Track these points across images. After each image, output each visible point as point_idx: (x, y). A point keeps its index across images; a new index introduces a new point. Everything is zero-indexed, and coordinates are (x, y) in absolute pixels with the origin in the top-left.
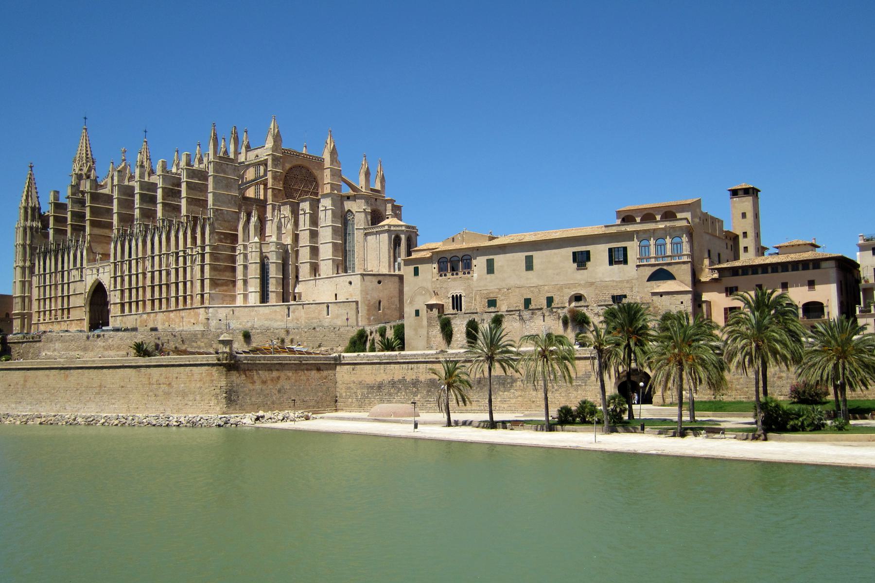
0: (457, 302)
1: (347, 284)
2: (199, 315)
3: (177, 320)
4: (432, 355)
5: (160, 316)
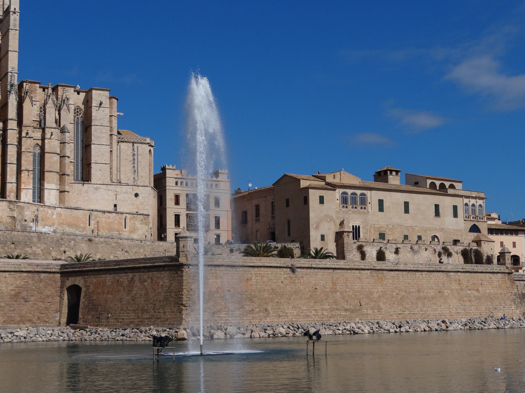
1: (140, 197)
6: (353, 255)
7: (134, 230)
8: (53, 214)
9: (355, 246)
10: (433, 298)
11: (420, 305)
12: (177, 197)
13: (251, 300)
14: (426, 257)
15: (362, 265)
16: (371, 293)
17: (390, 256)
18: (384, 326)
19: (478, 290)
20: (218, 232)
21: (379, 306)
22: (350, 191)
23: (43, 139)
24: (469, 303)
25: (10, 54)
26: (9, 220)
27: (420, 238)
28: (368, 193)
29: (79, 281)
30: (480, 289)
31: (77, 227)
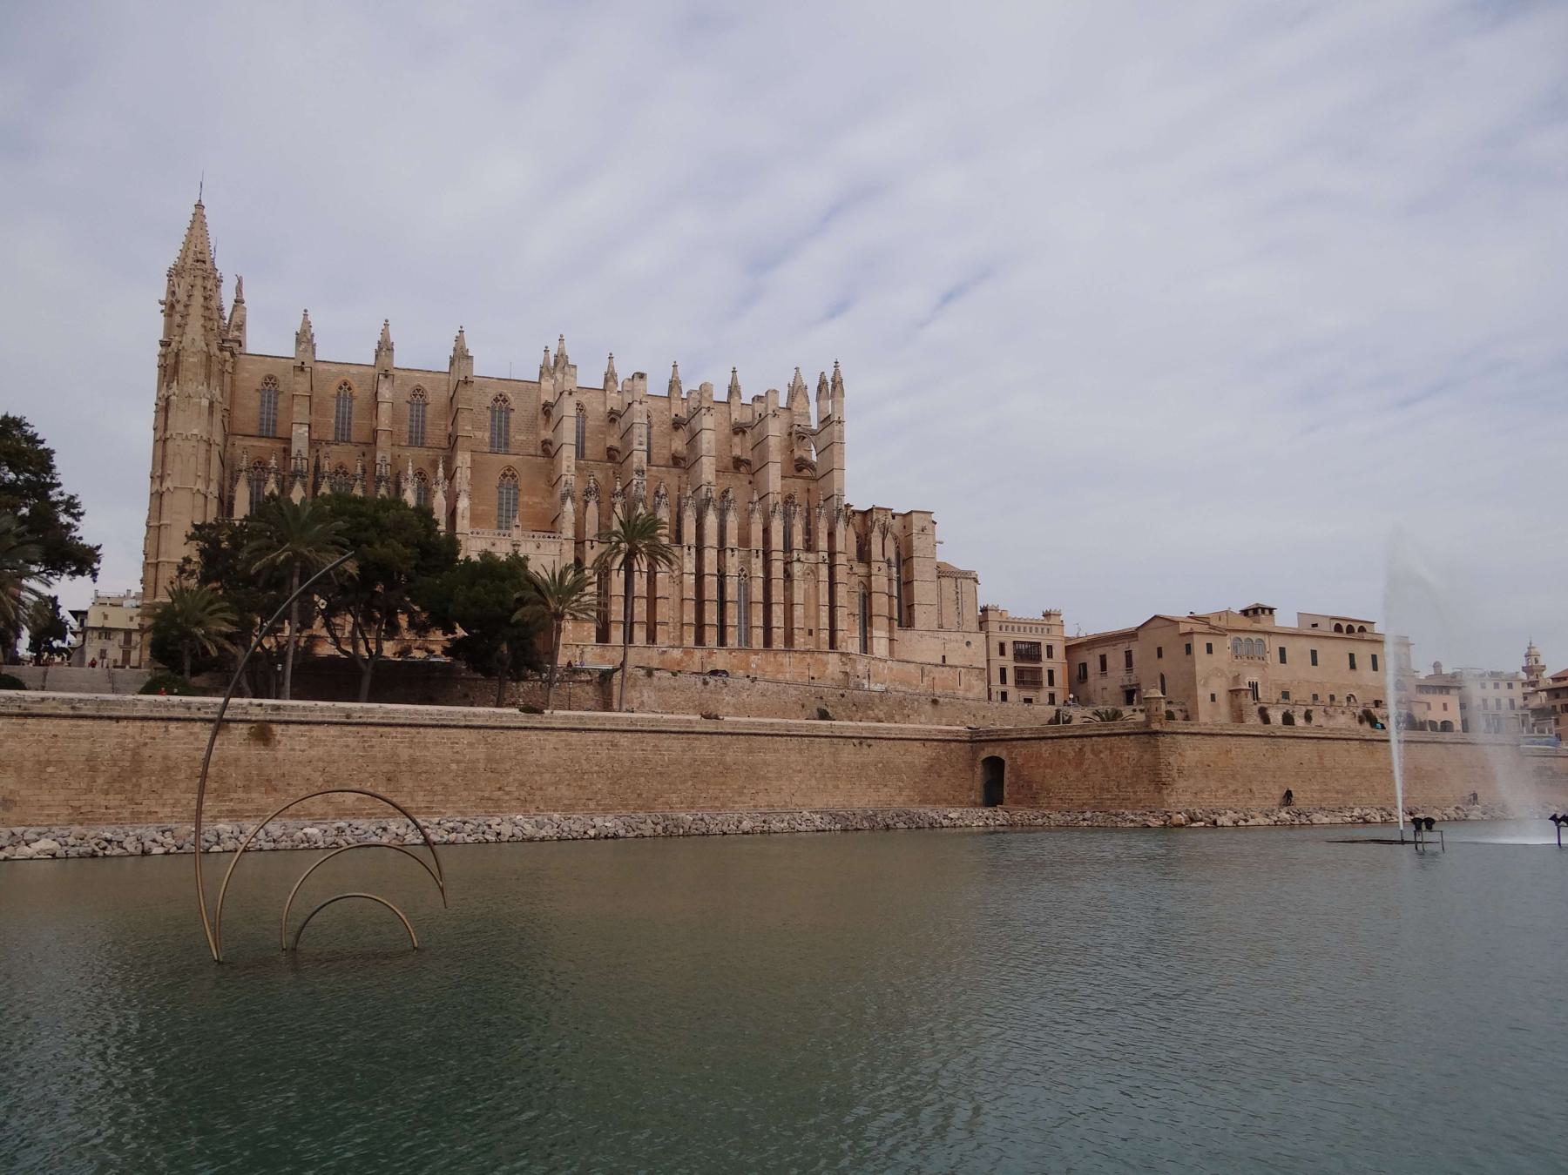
2: (825, 664)
6: (1253, 720)
7: (969, 688)
9: (1256, 708)
12: (1002, 646)
13: (1233, 777)
14: (1344, 722)
15: (1267, 729)
17: (1300, 721)
20: (1051, 690)
22: (1243, 636)
23: (869, 576)
25: (704, 459)
26: (842, 676)
27: (1332, 698)
28: (1266, 639)
29: (1000, 752)
31: (909, 684)
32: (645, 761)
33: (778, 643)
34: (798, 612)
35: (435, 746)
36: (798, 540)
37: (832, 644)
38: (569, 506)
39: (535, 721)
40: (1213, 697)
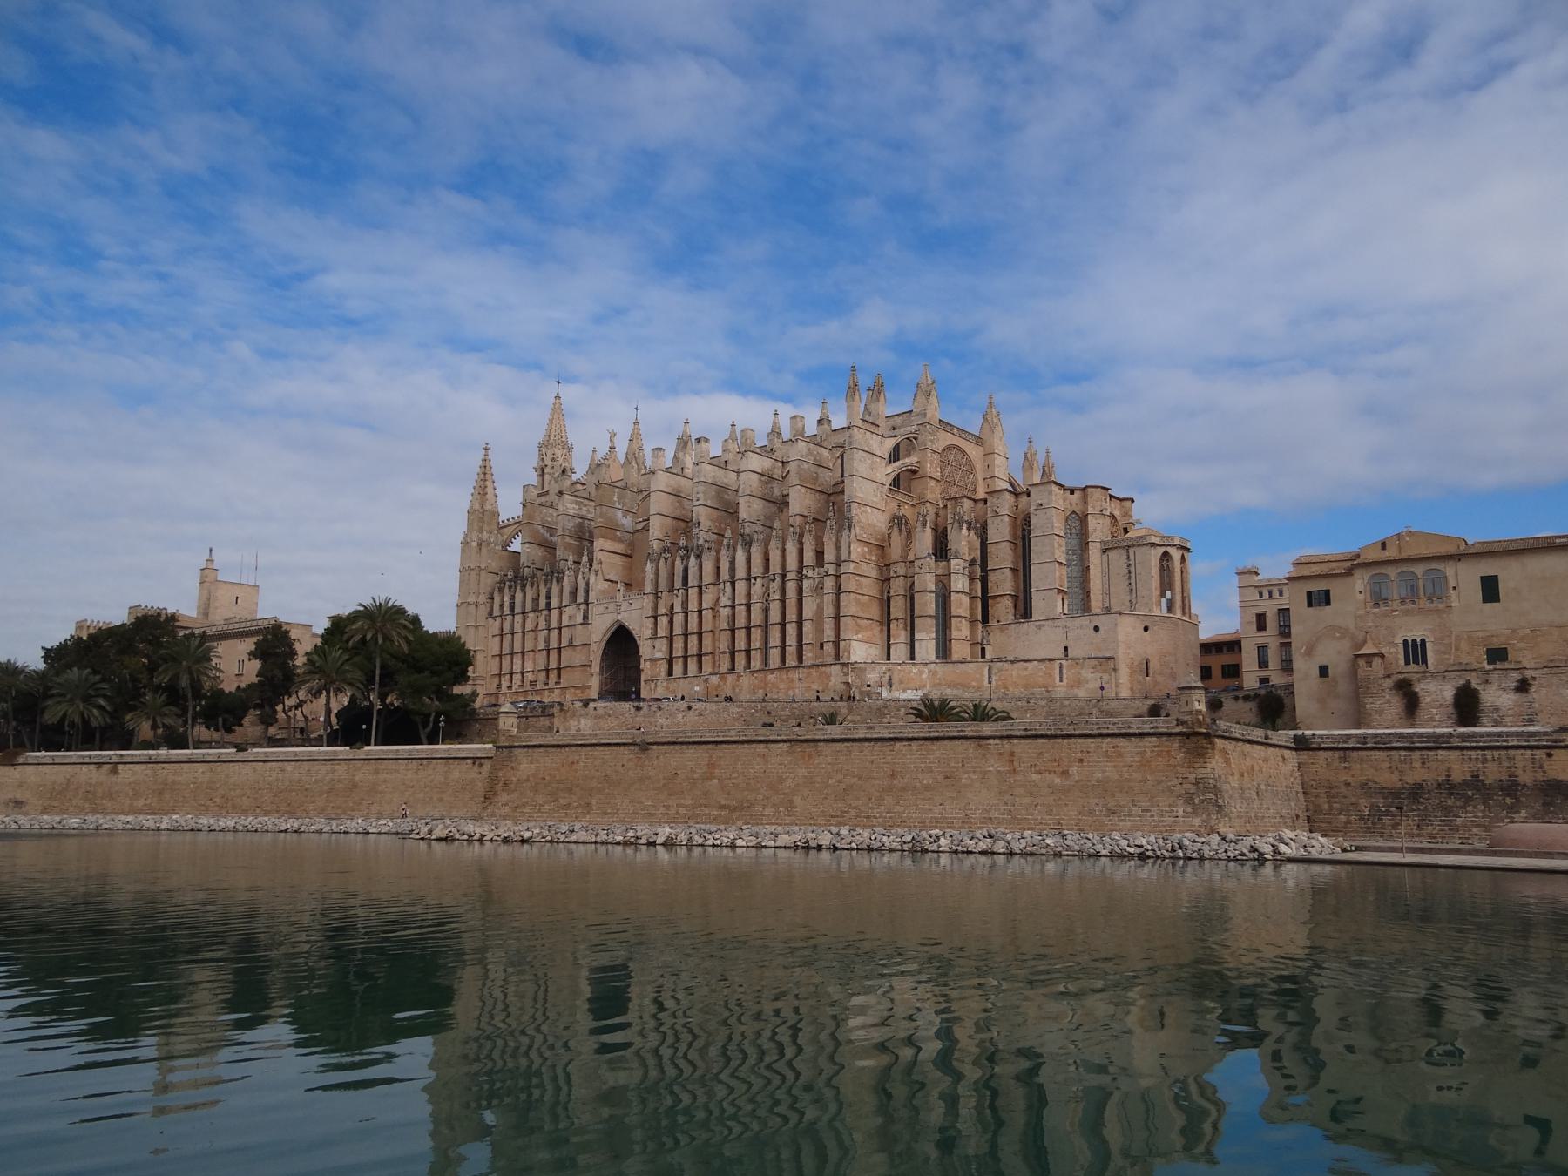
0: (1415, 651)
1: (1102, 630)
2: (828, 677)
3: (782, 686)
4: (1545, 734)
5: (746, 680)
8: (921, 673)
10: (927, 788)
11: (889, 800)
13: (570, 791)
16: (781, 780)
18: (1099, 847)
19: (1065, 773)
21: (791, 801)
22: (1419, 570)
24: (1027, 800)
30: (1074, 770)
32: (299, 781)
33: (791, 661)
34: (807, 627)
35: (187, 774)
36: (809, 558)
37: (837, 656)
38: (649, 567)
39: (241, 756)
40: (1324, 671)
